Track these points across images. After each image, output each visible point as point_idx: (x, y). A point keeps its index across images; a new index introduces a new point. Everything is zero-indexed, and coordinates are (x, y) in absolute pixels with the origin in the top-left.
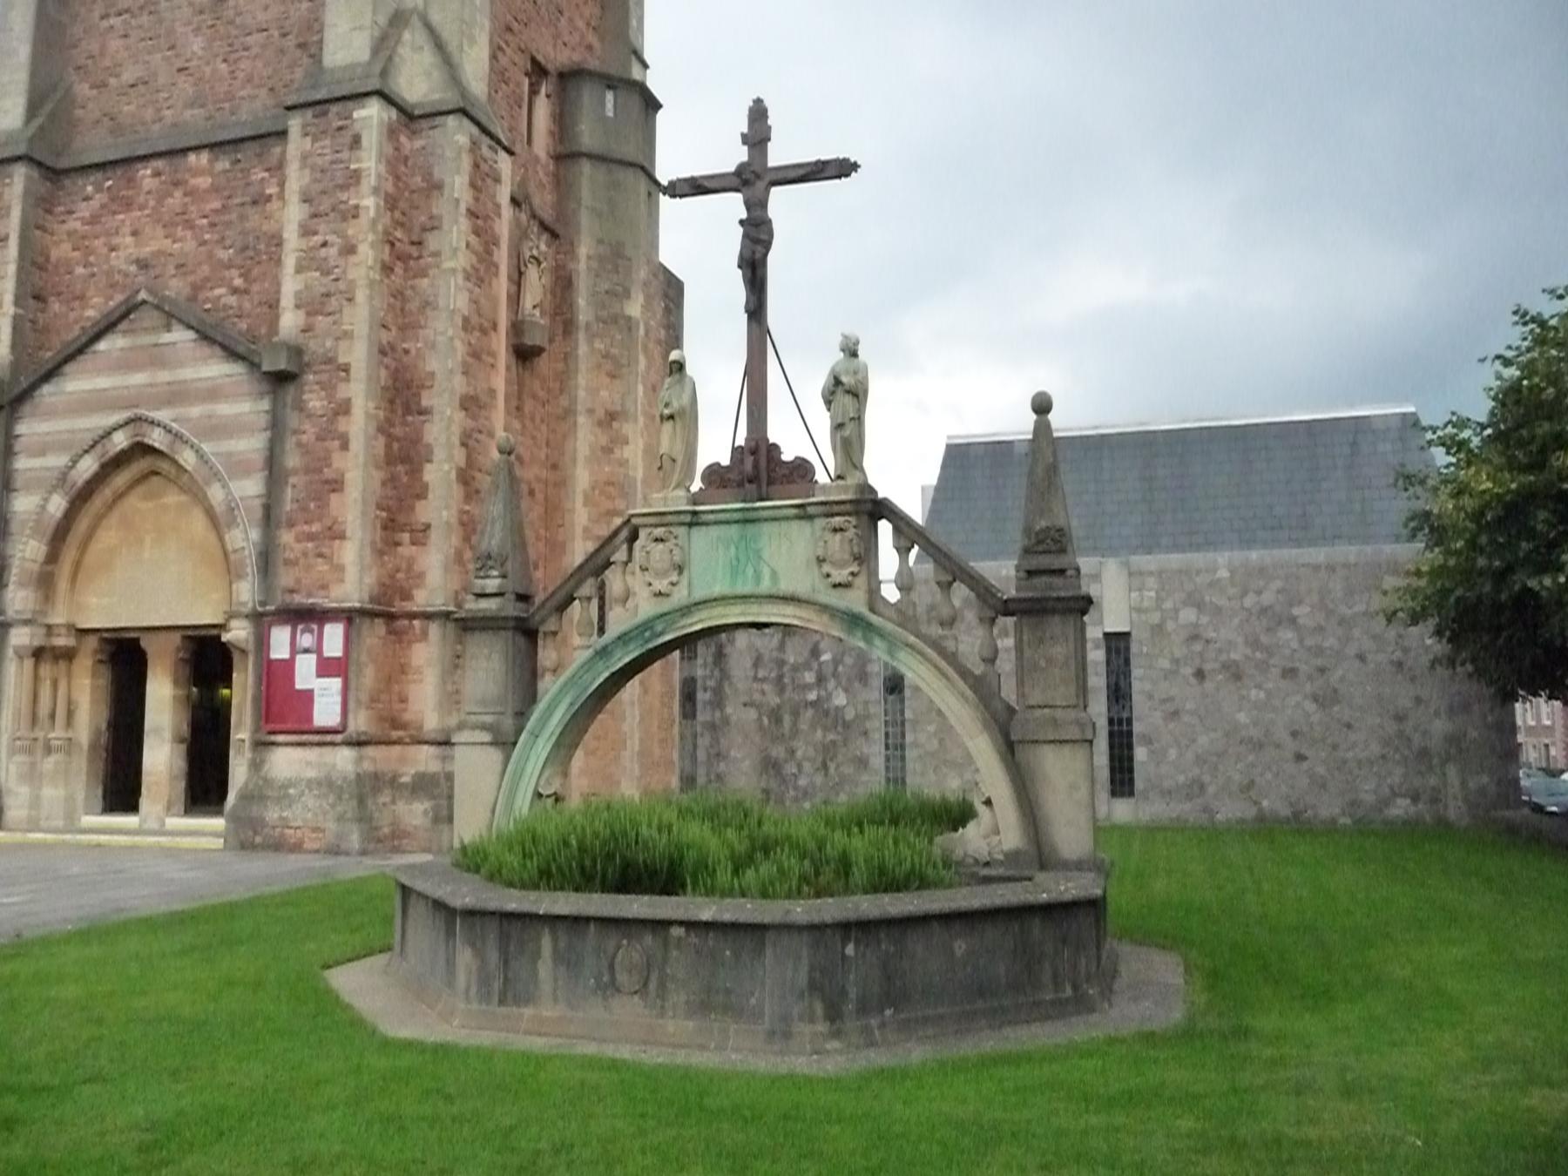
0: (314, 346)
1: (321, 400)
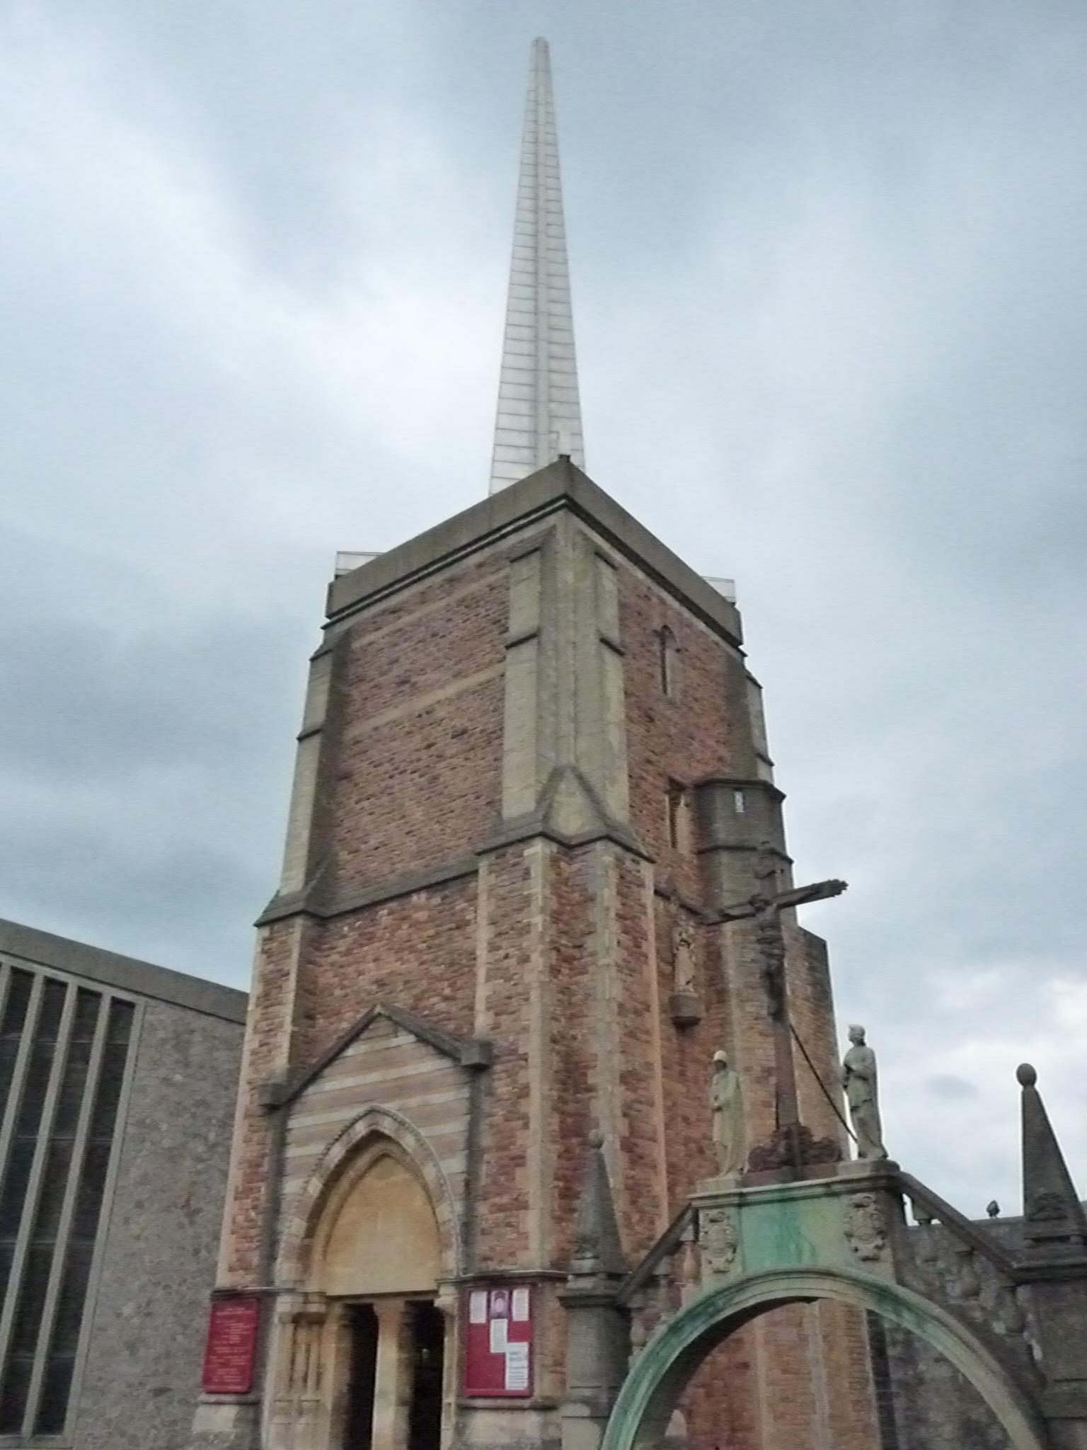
0: (502, 1042)
1: (508, 1086)
